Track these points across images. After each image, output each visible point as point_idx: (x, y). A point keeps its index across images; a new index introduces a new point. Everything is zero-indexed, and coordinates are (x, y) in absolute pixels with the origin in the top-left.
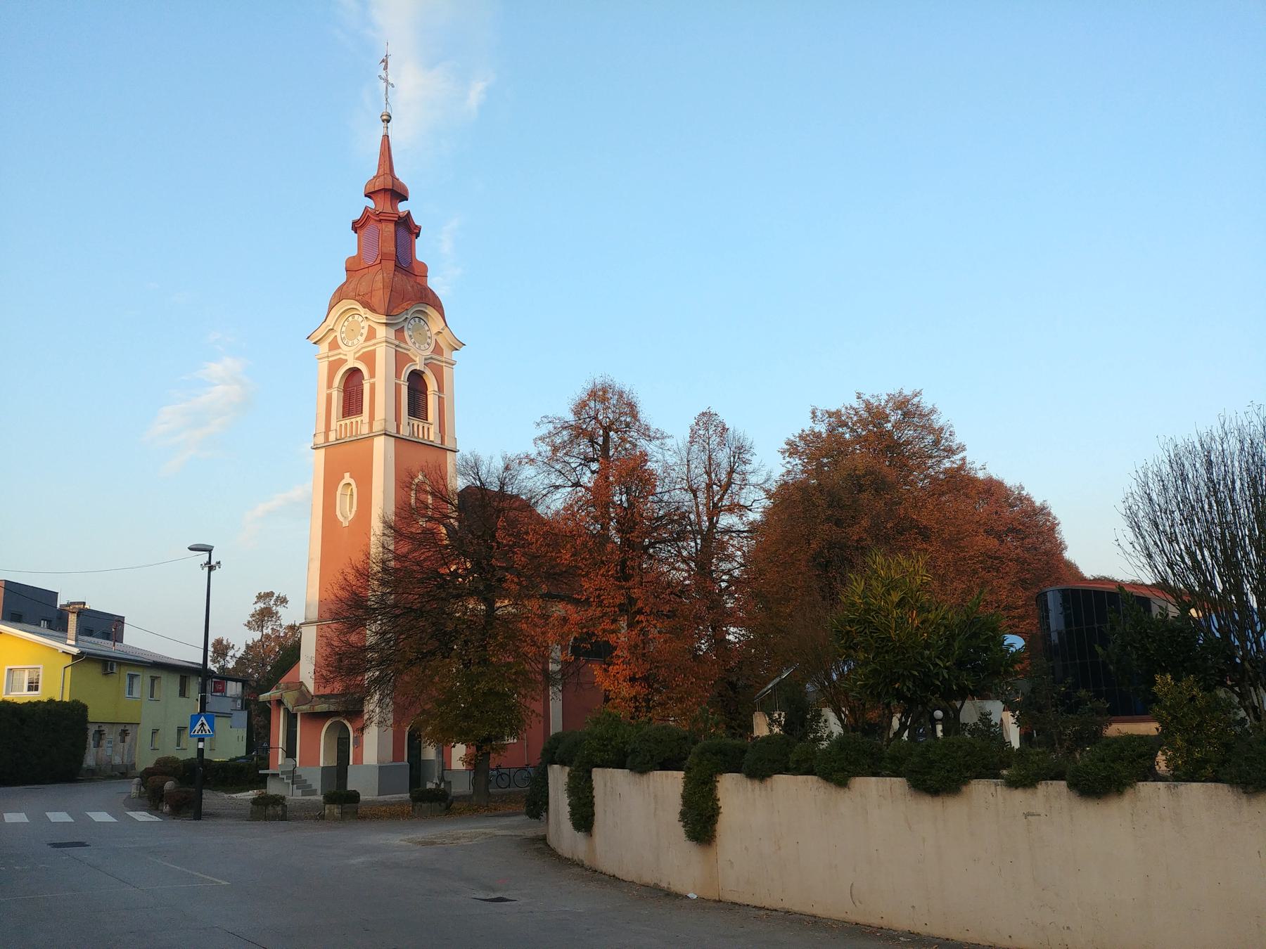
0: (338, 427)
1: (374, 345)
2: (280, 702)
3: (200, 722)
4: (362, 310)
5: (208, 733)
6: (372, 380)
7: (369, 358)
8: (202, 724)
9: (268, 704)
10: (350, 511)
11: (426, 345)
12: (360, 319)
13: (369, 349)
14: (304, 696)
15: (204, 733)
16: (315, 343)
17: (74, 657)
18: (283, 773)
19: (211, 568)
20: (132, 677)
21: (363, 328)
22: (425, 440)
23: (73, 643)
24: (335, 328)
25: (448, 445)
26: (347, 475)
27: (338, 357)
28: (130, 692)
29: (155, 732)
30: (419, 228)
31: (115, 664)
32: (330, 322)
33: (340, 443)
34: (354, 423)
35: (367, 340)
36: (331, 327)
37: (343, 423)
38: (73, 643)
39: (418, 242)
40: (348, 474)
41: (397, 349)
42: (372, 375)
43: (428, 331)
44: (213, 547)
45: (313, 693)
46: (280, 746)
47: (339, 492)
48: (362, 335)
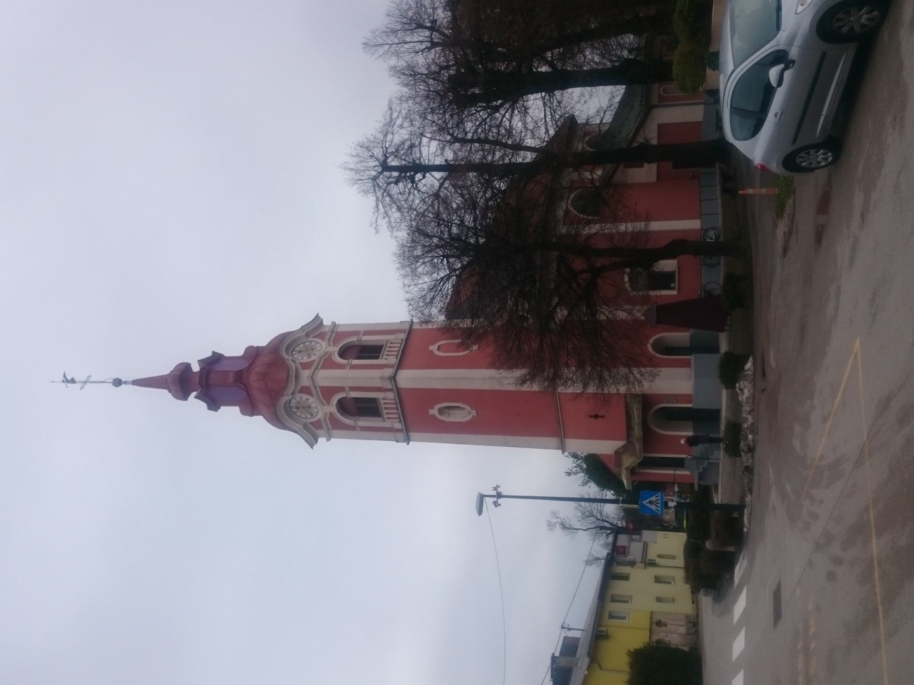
1: (315, 387)
3: (648, 505)
4: (285, 399)
5: (659, 498)
6: (347, 389)
7: (327, 393)
8: (650, 502)
9: (635, 484)
10: (463, 409)
11: (317, 345)
12: (294, 401)
13: (319, 391)
15: (659, 501)
19: (499, 495)
22: (401, 346)
25: (407, 327)
26: (431, 412)
27: (328, 420)
29: (659, 600)
30: (214, 353)
33: (404, 419)
34: (388, 416)
35: (310, 394)
36: (302, 427)
37: (386, 416)
42: (341, 389)
43: (304, 344)
44: (479, 493)
46: (672, 472)
48: (307, 399)
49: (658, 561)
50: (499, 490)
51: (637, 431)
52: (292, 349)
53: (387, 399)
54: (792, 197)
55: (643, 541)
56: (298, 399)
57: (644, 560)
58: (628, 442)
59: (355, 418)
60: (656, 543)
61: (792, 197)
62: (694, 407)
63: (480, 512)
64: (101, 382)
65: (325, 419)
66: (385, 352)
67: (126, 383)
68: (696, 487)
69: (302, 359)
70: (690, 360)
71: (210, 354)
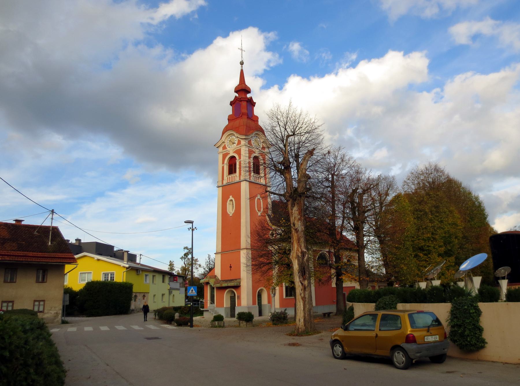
0: (227, 178)
1: (240, 147)
2: (208, 283)
3: (191, 290)
5: (194, 294)
7: (238, 152)
8: (192, 290)
10: (232, 210)
12: (235, 137)
14: (217, 281)
16: (217, 147)
17: (127, 268)
18: (210, 309)
19: (193, 230)
20: (146, 275)
21: (236, 141)
23: (126, 263)
24: (225, 141)
28: (146, 281)
29: (154, 296)
30: (255, 103)
31: (141, 271)
32: (223, 139)
33: (228, 185)
35: (238, 144)
36: (223, 141)
37: (229, 177)
38: (126, 263)
39: (255, 108)
40: (231, 196)
41: (249, 148)
42: (240, 158)
45: (220, 280)
47: (228, 204)
49: (172, 295)
50: (195, 229)
51: (225, 285)
52: (257, 136)
53: (236, 177)
54: (400, 318)
55: (180, 288)
56: (235, 139)
57: (172, 289)
58: (220, 281)
59: (228, 164)
60: (180, 294)
61: (400, 318)
62: (236, 307)
63: (185, 222)
64: (242, 56)
65: (227, 151)
66: (256, 175)
67: (242, 67)
68: (201, 309)
69: (253, 140)
70: (256, 304)
71: (254, 101)
